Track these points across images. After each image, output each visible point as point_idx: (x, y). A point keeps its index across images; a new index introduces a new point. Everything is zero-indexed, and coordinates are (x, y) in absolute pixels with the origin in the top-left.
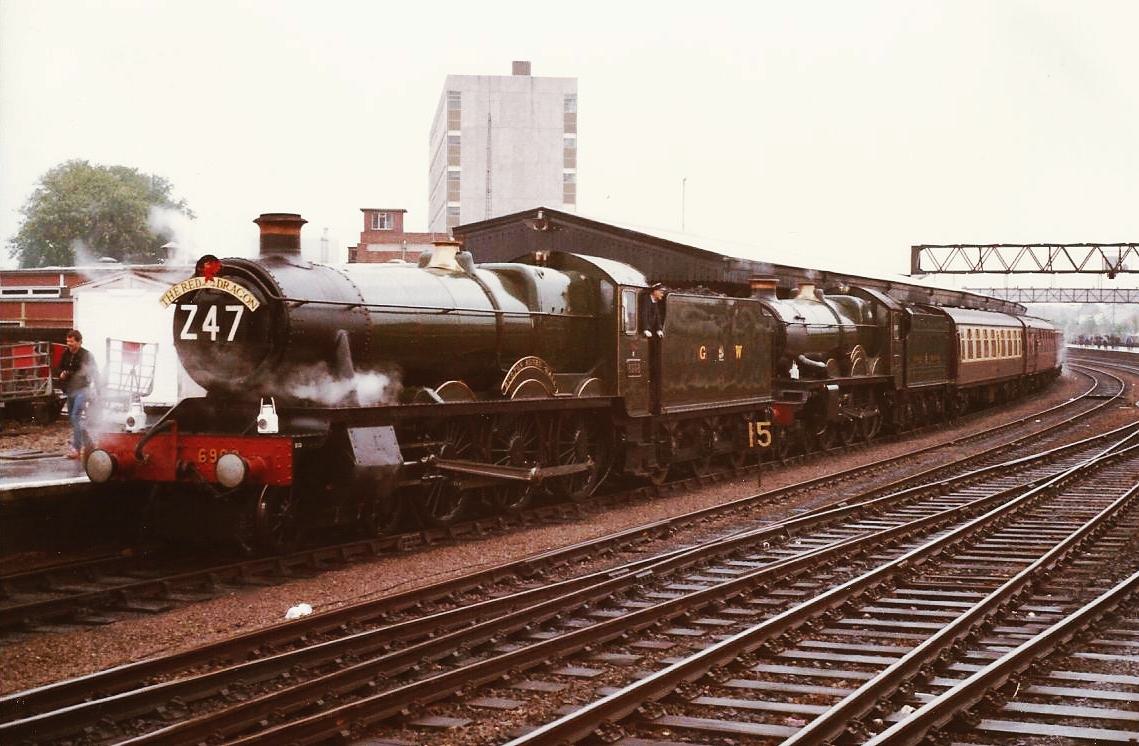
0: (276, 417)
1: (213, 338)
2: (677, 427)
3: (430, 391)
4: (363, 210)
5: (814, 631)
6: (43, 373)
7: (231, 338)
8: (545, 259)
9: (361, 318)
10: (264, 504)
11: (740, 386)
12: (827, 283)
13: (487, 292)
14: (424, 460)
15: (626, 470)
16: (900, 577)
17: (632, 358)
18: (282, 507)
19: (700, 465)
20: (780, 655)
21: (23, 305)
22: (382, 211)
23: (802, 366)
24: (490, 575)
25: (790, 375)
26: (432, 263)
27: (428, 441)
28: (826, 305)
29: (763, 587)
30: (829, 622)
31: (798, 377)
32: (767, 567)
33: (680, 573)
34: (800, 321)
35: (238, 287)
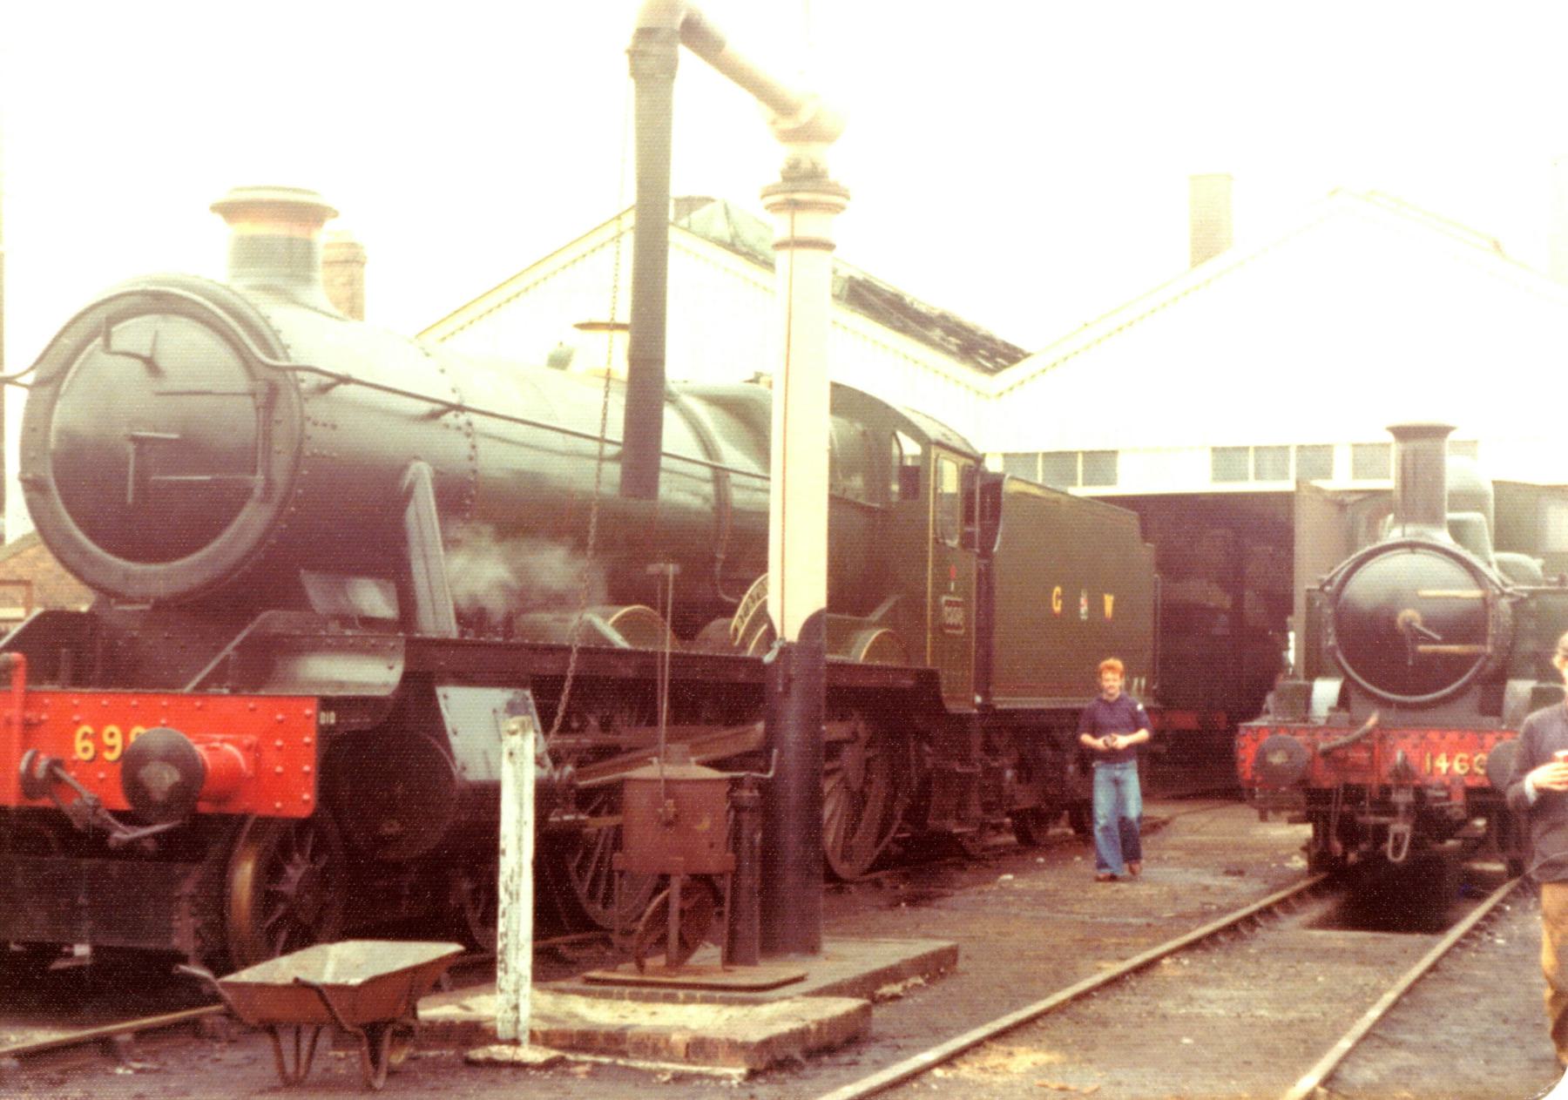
15: (933, 823)
21: (1080, 458)
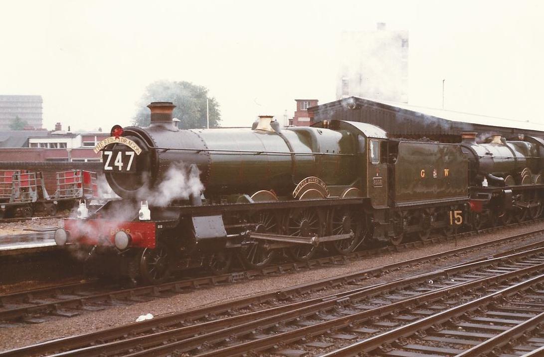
0: (149, 211)
1: (120, 169)
2: (407, 214)
3: (247, 196)
4: (296, 100)
5: (420, 338)
6: (79, 185)
7: (128, 169)
8: (328, 123)
9: (205, 158)
10: (144, 258)
11: (448, 191)
12: (509, 134)
13: (287, 142)
14: (243, 234)
16: (491, 305)
17: (377, 177)
18: (155, 259)
19: (424, 234)
20: (389, 354)
22: (306, 101)
23: (490, 181)
24: (258, 298)
25: (482, 184)
26: (258, 127)
27: (245, 223)
28: (508, 146)
29: (408, 309)
30: (430, 332)
31: (487, 186)
32: (474, 281)
33: (369, 299)
34: (489, 156)
35: (131, 142)
